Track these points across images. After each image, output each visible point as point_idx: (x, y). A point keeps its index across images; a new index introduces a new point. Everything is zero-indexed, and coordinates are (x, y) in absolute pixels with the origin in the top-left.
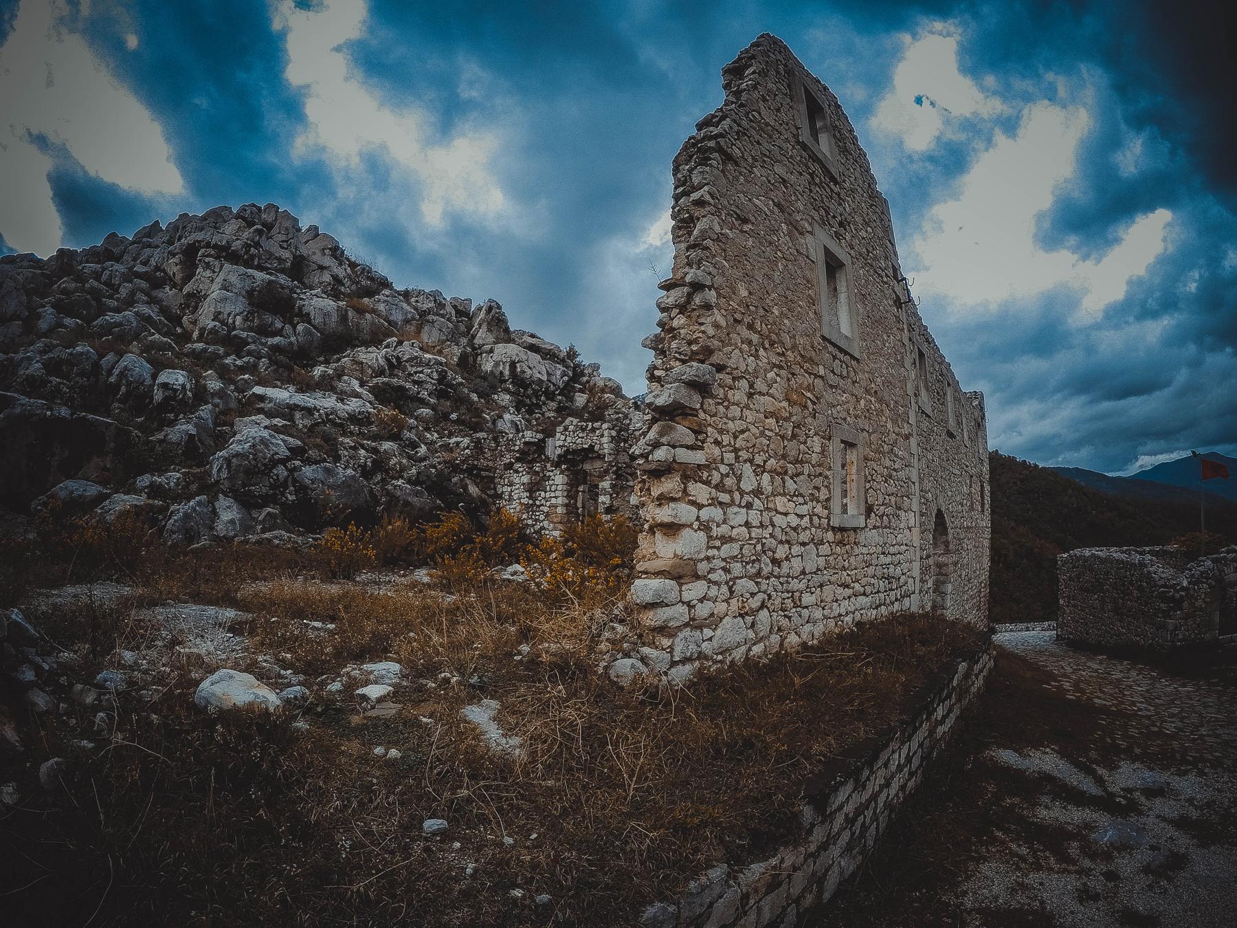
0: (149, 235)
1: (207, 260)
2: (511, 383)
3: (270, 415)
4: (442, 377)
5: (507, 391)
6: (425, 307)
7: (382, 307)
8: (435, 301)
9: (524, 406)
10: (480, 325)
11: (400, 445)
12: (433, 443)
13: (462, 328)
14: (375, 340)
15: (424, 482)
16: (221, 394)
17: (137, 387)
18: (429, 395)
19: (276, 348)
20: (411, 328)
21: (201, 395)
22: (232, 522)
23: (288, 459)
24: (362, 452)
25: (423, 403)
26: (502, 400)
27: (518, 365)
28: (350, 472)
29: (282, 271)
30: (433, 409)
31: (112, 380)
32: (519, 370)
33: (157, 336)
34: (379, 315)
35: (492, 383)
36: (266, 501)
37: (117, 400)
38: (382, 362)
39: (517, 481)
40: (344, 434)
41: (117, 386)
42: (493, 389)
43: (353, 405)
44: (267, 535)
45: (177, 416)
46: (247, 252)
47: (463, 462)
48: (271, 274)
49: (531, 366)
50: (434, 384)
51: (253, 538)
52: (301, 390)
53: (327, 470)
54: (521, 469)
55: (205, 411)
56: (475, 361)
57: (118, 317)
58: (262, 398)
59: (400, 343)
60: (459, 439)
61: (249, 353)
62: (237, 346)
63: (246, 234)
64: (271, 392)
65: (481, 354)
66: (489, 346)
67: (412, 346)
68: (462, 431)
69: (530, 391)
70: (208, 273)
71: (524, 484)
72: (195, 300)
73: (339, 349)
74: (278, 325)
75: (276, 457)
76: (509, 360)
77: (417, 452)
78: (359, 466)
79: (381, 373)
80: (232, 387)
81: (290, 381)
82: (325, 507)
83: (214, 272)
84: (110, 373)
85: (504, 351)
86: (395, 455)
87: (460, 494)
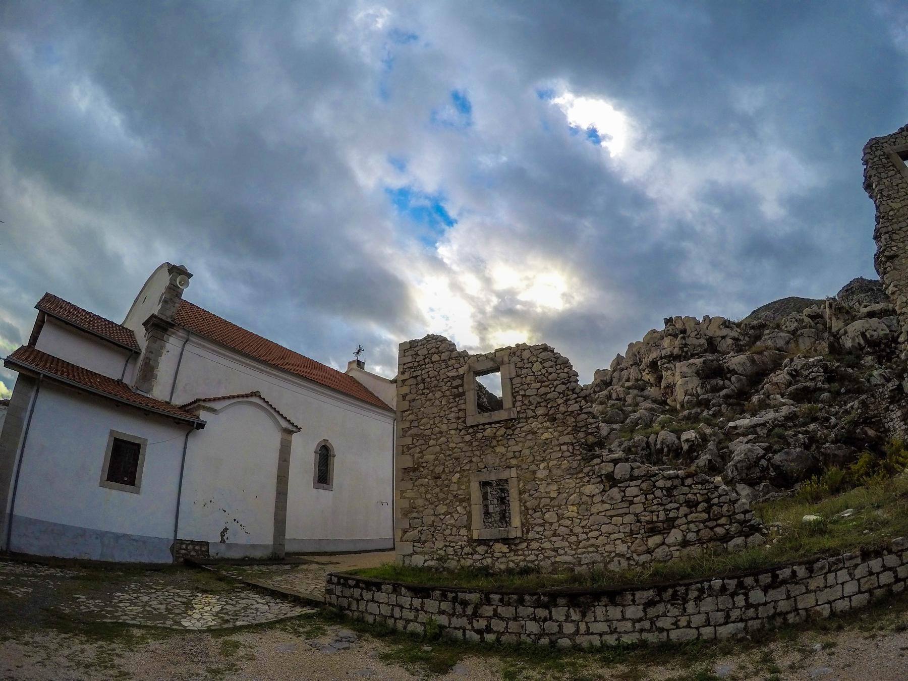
0: (618, 364)
1: (665, 366)
2: (868, 347)
3: (744, 435)
4: (826, 369)
5: (868, 353)
6: (793, 328)
7: (769, 343)
8: (796, 320)
9: (884, 358)
10: (830, 319)
11: (819, 423)
12: (837, 413)
13: (820, 327)
14: (777, 365)
15: (841, 440)
16: (714, 434)
17: (672, 446)
18: (823, 384)
19: (727, 397)
20: (792, 345)
21: (705, 439)
22: (748, 495)
23: (765, 455)
24: (800, 436)
25: (822, 390)
26: (868, 362)
27: (866, 333)
28: (798, 450)
29: (705, 351)
30: (829, 392)
31: (658, 446)
32: (868, 336)
33: (662, 416)
34: (770, 349)
35: (857, 352)
36: (760, 480)
37: (664, 456)
38: (788, 377)
39: (894, 416)
40: (786, 430)
41: (662, 449)
42: (859, 358)
43: (784, 411)
44: (767, 497)
45: (698, 452)
46: (683, 351)
47: (859, 418)
48: (701, 357)
49: (875, 329)
50: (822, 376)
51: (761, 500)
52: (753, 415)
53: (787, 453)
54: (894, 409)
55: (711, 445)
56: (839, 343)
57: (637, 415)
58: (735, 428)
59: (792, 360)
60: (852, 404)
61: (714, 405)
62: (706, 404)
63: (678, 342)
64: (739, 423)
65: (840, 337)
66: (843, 329)
67: (799, 358)
68: (851, 397)
69: (883, 346)
70: (669, 372)
71: (899, 417)
72: (670, 388)
73: (760, 381)
74: (721, 383)
75: (759, 456)
76: (859, 333)
77: (830, 423)
78: (802, 444)
79: (790, 384)
80: (717, 428)
81: (742, 412)
82: (792, 472)
83: (672, 370)
84: (655, 444)
85: (854, 329)
86: (819, 430)
87: (864, 439)
